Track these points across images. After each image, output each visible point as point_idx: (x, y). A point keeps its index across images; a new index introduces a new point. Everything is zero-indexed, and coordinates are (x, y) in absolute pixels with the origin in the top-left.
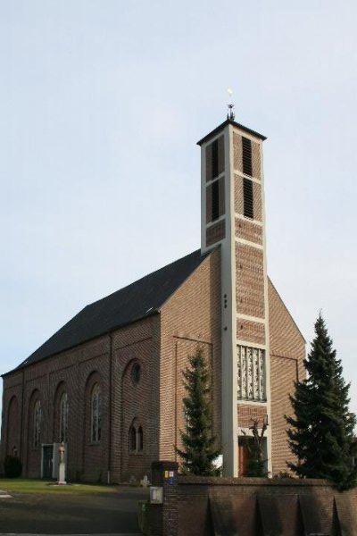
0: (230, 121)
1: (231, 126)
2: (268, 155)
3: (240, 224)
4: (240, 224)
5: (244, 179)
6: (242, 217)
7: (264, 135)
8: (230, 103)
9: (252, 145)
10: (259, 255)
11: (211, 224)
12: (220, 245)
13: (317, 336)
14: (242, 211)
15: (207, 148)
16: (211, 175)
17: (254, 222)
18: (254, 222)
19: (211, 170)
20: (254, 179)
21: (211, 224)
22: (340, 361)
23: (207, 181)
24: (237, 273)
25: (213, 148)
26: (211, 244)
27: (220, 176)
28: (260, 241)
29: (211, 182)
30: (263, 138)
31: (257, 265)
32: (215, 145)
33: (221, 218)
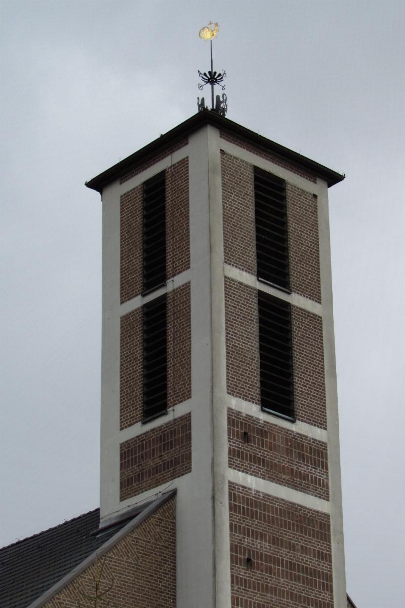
0: (210, 118)
1: (211, 142)
2: (188, 270)
3: (242, 430)
4: (242, 430)
5: (261, 294)
6: (252, 409)
7: (339, 170)
8: (218, 70)
9: (289, 194)
10: (319, 529)
11: (137, 429)
12: (174, 494)
13: (226, 117)
14: (256, 392)
15: (125, 199)
16: (138, 278)
17: (301, 428)
18: (301, 428)
19: (137, 262)
20: (297, 300)
21: (137, 429)
22: (207, 107)
23: (125, 296)
24: (234, 579)
25: (146, 198)
26: (136, 492)
27: (174, 284)
28: (322, 489)
29: (137, 302)
30: (333, 178)
31: (313, 562)
32: (155, 192)
33: (178, 411)
